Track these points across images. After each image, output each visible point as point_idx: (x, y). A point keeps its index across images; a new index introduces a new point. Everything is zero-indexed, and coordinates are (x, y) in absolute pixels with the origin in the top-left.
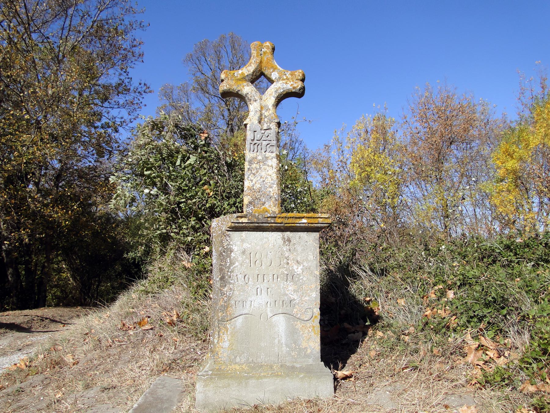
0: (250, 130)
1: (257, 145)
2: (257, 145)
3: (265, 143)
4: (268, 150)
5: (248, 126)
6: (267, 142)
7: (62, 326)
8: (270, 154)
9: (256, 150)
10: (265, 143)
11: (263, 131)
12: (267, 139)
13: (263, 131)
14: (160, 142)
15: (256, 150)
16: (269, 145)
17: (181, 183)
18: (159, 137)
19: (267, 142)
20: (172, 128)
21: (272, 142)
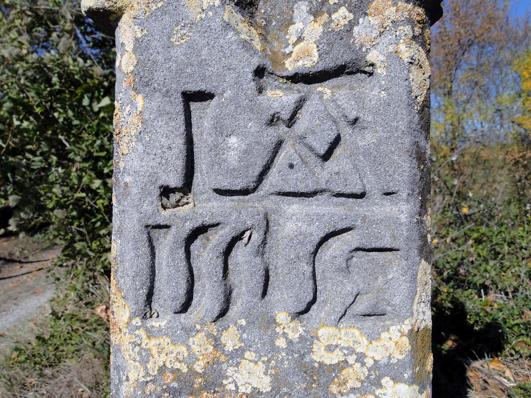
0: (143, 83)
1: (217, 238)
2: (217, 238)
3: (297, 221)
4: (335, 291)
5: (126, 34)
6: (329, 211)
7: (18, 267)
8: (351, 335)
9: (206, 300)
10: (297, 221)
11: (280, 97)
12: (325, 174)
13: (280, 97)
14: (48, 55)
15: (206, 300)
16: (336, 247)
17: (92, 144)
18: (45, 44)
19: (329, 211)
20: (68, 26)
21: (378, 209)
